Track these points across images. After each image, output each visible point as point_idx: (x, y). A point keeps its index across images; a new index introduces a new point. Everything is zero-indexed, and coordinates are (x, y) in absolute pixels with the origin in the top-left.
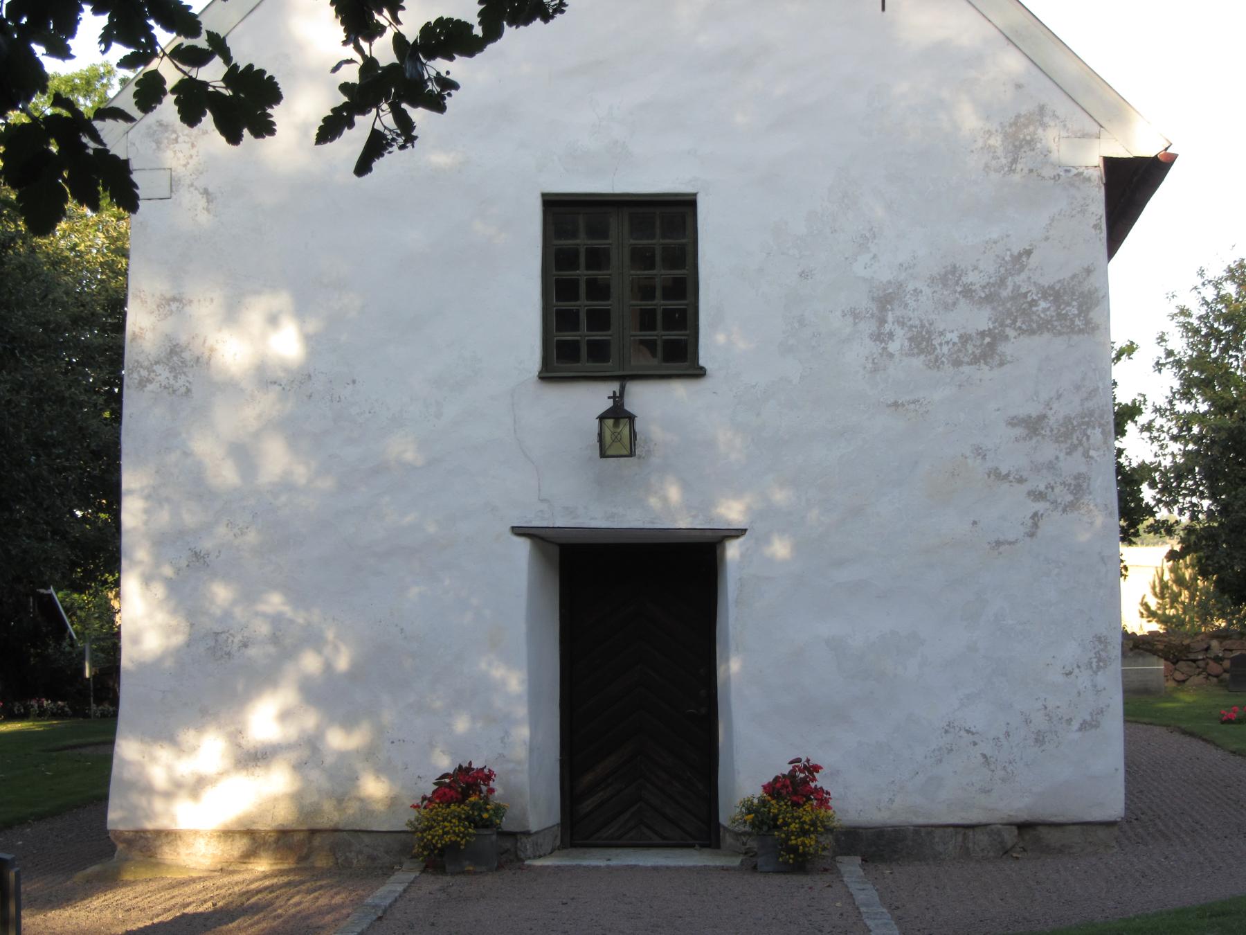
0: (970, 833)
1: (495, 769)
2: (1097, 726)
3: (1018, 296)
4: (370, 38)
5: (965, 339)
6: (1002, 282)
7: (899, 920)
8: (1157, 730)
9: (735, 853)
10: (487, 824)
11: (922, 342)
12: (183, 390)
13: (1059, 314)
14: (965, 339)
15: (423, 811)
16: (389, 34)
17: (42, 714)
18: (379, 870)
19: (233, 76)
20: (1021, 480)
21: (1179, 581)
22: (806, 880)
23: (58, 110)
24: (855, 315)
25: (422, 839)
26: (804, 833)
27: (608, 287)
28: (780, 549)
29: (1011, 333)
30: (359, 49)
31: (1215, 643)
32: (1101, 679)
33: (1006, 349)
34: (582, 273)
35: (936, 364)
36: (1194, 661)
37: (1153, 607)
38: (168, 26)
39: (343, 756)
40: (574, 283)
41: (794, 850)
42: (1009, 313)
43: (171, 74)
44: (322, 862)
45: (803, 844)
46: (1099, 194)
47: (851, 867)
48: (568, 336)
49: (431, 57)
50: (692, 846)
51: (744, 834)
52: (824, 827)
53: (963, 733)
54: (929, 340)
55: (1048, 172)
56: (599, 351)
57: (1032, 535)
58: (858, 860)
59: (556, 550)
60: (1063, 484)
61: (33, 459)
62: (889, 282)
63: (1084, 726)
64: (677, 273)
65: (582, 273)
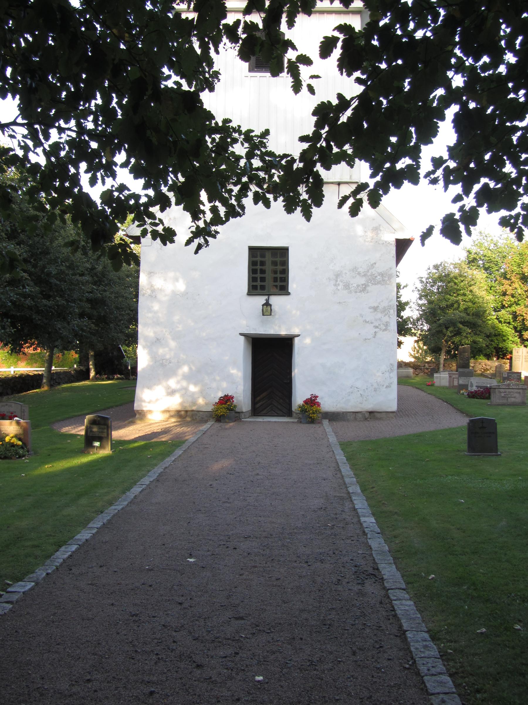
0: (357, 414)
1: (234, 396)
2: (390, 387)
3: (372, 275)
4: (198, 221)
5: (358, 286)
6: (368, 271)
7: (337, 436)
8: (409, 387)
9: (296, 418)
10: (232, 410)
11: (347, 286)
12: (154, 296)
13: (383, 280)
14: (358, 286)
15: (216, 406)
16: (203, 219)
17: (118, 379)
18: (203, 421)
19: (164, 229)
20: (372, 323)
21: (419, 347)
22: (314, 425)
23: (121, 242)
24: (330, 279)
25: (215, 413)
26: (314, 413)
27: (272, 264)
28: (308, 341)
29: (370, 284)
30: (195, 223)
31: (426, 365)
32: (391, 375)
33: (368, 288)
34: (259, 267)
35: (350, 292)
36: (421, 369)
37: (412, 354)
38: (149, 218)
39: (193, 393)
40: (256, 270)
41: (311, 418)
42: (370, 279)
43: (149, 229)
44: (188, 419)
45: (313, 416)
46: (394, 248)
47: (326, 422)
48: (255, 284)
49: (213, 226)
50: (285, 416)
51: (298, 413)
52: (319, 412)
53: (355, 388)
54: (349, 286)
55: (381, 242)
56: (263, 288)
57: (374, 337)
58: (328, 420)
59: (251, 339)
60: (383, 324)
61: (115, 312)
62: (339, 271)
63: (387, 387)
64: (284, 267)
65: (259, 267)
